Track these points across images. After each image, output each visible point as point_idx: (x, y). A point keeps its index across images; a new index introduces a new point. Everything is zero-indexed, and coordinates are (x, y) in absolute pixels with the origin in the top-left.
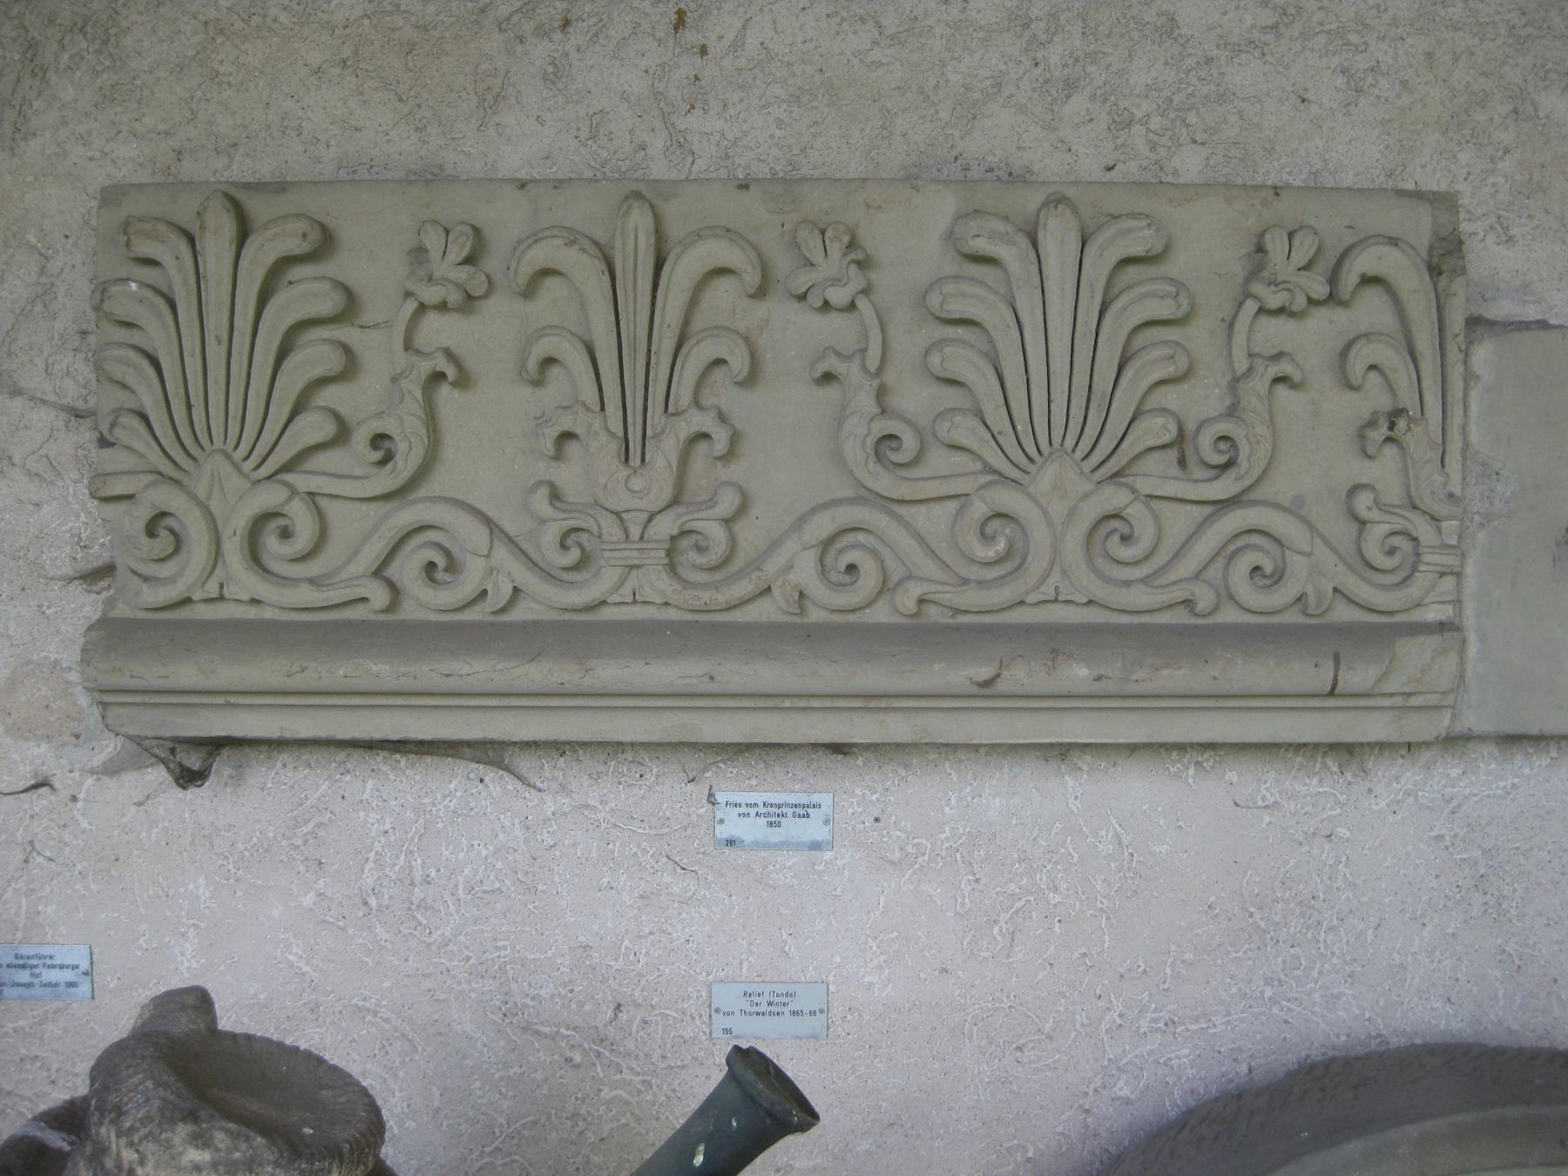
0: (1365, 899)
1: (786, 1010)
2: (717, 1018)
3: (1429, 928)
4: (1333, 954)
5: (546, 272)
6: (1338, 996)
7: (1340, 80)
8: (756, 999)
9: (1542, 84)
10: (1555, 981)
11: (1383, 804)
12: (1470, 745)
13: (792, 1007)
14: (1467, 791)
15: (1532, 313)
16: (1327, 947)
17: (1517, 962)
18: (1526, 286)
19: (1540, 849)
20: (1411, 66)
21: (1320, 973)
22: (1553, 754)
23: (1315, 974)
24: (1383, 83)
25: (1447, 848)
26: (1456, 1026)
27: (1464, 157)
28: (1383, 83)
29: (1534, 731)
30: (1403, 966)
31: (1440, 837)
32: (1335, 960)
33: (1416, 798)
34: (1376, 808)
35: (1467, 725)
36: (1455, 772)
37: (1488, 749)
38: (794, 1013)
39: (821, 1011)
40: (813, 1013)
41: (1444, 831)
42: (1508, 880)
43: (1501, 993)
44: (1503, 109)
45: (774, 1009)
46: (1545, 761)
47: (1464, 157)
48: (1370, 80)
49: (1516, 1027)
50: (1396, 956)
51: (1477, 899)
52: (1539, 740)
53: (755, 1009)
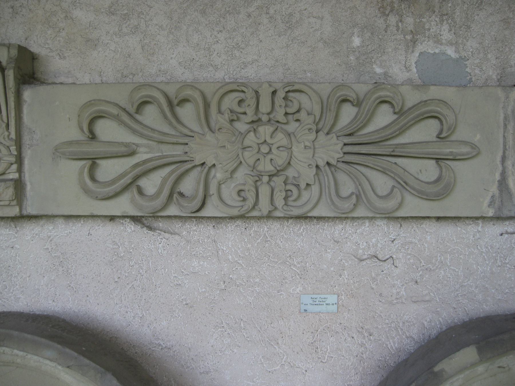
0: (25, 268)
1: (324, 303)
2: (302, 306)
3: (46, 277)
4: (17, 285)
5: (145, 103)
6: (19, 298)
7: (11, 10)
8: (315, 300)
9: (74, 7)
10: (88, 296)
11: (29, 238)
12: (56, 219)
13: (327, 302)
14: (55, 234)
15: (70, 81)
16: (14, 282)
17: (75, 290)
18: (69, 72)
19: (79, 253)
20: (33, 4)
21: (13, 290)
22: (82, 223)
23: (11, 291)
24: (24, 10)
25: (49, 252)
26: (57, 309)
27: (49, 32)
28: (24, 10)
29: (50, 213)
30: (38, 289)
31: (48, 249)
32: (17, 287)
33: (39, 236)
34: (27, 239)
35: (28, 212)
36: (51, 228)
37: (61, 220)
38: (327, 304)
39: (336, 304)
40: (333, 304)
41: (48, 247)
42: (70, 263)
43: (70, 299)
44: (62, 16)
45: (321, 303)
46: (80, 225)
47: (49, 32)
48: (20, 10)
49: (77, 311)
50: (36, 286)
51: (61, 269)
52: (78, 217)
53: (314, 303)
